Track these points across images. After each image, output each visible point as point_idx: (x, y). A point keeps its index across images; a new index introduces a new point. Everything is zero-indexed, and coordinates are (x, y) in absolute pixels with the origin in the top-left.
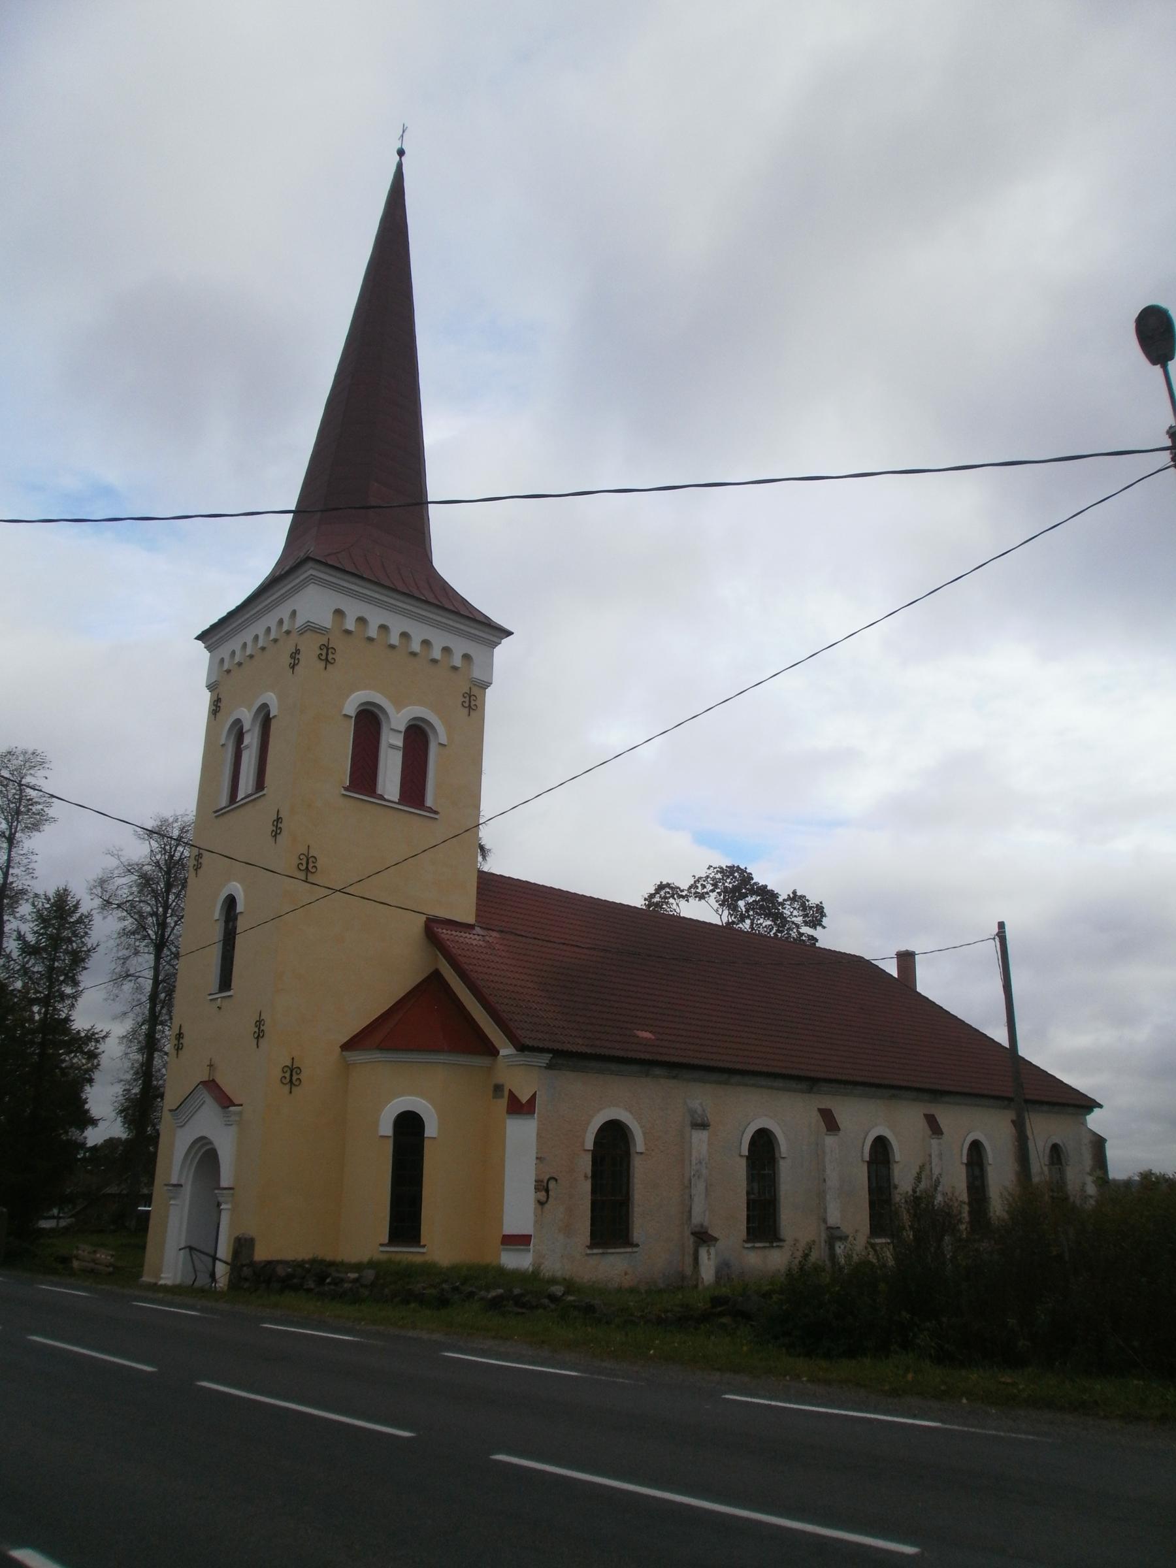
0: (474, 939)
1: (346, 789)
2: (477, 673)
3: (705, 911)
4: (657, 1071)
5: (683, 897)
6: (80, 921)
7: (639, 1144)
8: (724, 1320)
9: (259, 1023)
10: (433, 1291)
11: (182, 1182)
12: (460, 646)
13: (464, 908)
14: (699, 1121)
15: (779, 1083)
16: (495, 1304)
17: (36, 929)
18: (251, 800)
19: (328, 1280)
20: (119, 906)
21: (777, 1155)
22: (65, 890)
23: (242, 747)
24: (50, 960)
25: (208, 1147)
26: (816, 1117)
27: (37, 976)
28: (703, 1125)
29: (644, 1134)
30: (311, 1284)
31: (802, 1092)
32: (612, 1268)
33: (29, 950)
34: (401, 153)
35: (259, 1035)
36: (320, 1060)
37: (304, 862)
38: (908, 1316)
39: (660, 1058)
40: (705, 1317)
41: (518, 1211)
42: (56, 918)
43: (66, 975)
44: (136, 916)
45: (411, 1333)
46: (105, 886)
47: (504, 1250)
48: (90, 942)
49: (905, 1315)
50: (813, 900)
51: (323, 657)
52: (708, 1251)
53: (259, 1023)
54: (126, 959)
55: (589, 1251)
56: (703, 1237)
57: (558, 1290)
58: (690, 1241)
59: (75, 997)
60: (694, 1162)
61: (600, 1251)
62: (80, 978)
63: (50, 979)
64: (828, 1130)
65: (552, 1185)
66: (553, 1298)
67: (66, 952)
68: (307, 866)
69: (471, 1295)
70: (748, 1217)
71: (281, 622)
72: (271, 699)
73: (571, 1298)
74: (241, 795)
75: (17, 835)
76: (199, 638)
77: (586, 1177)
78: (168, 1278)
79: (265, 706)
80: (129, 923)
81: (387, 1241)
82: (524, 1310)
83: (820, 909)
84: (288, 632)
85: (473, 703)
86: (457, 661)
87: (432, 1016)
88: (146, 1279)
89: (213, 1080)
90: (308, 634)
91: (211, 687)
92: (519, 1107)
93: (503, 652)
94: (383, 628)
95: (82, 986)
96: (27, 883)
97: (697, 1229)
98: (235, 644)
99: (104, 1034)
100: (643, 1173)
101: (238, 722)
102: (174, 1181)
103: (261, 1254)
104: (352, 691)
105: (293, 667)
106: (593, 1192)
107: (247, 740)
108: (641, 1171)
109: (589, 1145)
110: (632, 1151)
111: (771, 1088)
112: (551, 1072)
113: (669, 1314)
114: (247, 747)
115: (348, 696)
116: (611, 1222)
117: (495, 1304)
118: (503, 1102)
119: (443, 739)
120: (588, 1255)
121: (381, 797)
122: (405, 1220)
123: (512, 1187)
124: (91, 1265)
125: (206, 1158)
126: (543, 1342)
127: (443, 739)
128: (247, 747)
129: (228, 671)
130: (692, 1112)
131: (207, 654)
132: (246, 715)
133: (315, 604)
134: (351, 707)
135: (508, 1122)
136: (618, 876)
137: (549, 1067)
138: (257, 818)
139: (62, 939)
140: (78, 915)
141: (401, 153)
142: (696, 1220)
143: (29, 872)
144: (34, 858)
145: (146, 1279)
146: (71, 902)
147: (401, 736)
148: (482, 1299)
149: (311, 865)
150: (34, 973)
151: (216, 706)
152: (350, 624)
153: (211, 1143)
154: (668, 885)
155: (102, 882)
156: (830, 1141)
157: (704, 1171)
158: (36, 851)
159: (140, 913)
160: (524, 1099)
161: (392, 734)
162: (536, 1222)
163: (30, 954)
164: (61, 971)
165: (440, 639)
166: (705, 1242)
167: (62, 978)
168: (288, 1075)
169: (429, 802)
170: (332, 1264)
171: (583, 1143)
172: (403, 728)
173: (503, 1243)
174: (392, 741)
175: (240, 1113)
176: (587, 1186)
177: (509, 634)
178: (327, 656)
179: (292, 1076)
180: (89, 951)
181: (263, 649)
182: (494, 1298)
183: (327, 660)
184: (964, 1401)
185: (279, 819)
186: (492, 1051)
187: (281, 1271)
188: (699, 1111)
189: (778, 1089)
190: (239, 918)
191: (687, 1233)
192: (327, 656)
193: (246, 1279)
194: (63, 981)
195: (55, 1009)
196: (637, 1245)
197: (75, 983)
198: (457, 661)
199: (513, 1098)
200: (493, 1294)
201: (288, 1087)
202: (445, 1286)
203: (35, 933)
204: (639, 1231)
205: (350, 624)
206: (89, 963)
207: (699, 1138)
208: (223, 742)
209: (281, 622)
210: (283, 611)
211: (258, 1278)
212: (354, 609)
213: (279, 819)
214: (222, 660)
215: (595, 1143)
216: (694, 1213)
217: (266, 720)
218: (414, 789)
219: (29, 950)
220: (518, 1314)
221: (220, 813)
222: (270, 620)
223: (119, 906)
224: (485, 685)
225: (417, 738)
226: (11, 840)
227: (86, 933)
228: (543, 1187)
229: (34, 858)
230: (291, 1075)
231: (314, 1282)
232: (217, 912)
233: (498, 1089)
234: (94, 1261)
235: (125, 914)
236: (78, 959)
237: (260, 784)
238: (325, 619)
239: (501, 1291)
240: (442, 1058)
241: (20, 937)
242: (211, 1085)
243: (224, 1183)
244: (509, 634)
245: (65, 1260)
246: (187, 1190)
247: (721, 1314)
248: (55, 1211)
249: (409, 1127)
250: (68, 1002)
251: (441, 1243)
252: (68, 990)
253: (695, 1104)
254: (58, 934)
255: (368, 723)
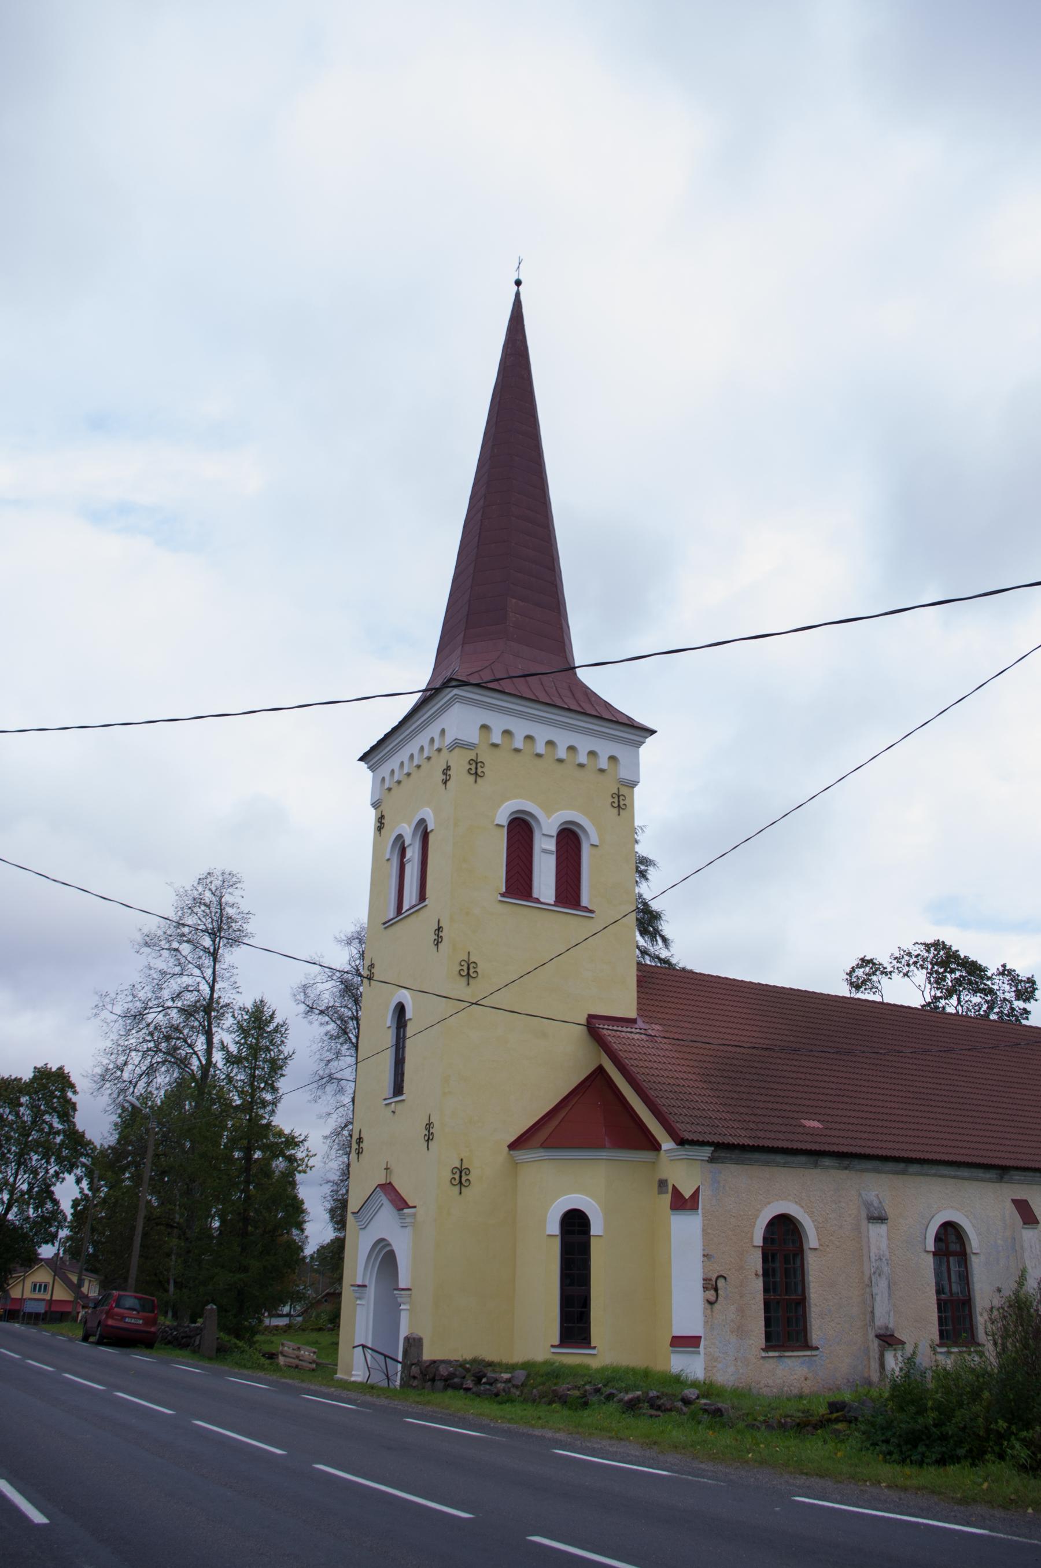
0: (633, 1036)
1: (503, 895)
2: (624, 773)
3: (909, 991)
4: (827, 1162)
5: (886, 974)
6: (276, 1030)
7: (812, 1239)
8: (840, 1426)
9: (429, 1126)
10: (577, 1393)
11: (367, 1283)
12: (605, 749)
13: (624, 1003)
14: (876, 1215)
15: (965, 1172)
16: (632, 1406)
17: (237, 1039)
18: (415, 910)
19: (484, 1380)
20: (322, 1012)
21: (968, 1251)
22: (262, 1001)
23: (406, 861)
24: (251, 1068)
25: (388, 1248)
26: (1010, 1208)
27: (240, 1084)
28: (881, 1219)
29: (817, 1229)
30: (469, 1383)
31: (990, 1181)
32: (789, 1375)
33: (232, 1060)
34: (518, 283)
35: (429, 1138)
36: (488, 1158)
37: (465, 968)
38: (1005, 1425)
39: (827, 1148)
40: (822, 1423)
41: (687, 1313)
42: (254, 1028)
43: (266, 1083)
44: (339, 1022)
45: (537, 1432)
46: (308, 991)
47: (673, 1352)
48: (286, 1050)
49: (1002, 1424)
50: (1023, 974)
51: (473, 771)
52: (895, 1356)
53: (429, 1126)
54: (329, 1061)
55: (764, 1354)
56: (888, 1340)
57: (691, 1393)
58: (875, 1345)
59: (274, 1103)
60: (873, 1260)
61: (776, 1354)
62: (277, 1085)
63: (252, 1085)
64: (1025, 1223)
65: (721, 1283)
66: (686, 1402)
67: (265, 1061)
68: (468, 971)
69: (610, 1397)
70: (940, 1319)
71: (432, 740)
72: (428, 813)
73: (703, 1401)
74: (406, 906)
75: (220, 951)
76: (361, 759)
77: (756, 1275)
78: (358, 1375)
79: (422, 821)
80: (332, 1027)
81: (557, 1342)
82: (659, 1413)
83: (1031, 981)
84: (439, 750)
85: (622, 802)
86: (603, 763)
87: (597, 1114)
88: (339, 1375)
89: (390, 1183)
90: (457, 750)
91: (376, 805)
92: (682, 1203)
93: (648, 751)
94: (529, 738)
95: (281, 1092)
96: (232, 996)
97: (882, 1332)
98: (393, 763)
99: (302, 1138)
100: (819, 1271)
101: (400, 837)
102: (359, 1282)
103: (428, 1354)
104: (503, 802)
105: (445, 782)
106: (766, 1290)
107: (409, 854)
108: (815, 1267)
109: (759, 1240)
110: (805, 1247)
111: (954, 1177)
112: (714, 1165)
113: (788, 1420)
114: (409, 861)
115: (499, 807)
116: (786, 1321)
117: (632, 1406)
118: (667, 1198)
119: (594, 839)
120: (763, 1358)
121: (538, 901)
122: (575, 1323)
123: (677, 1285)
124: (296, 1361)
125: (386, 1259)
126: (655, 1443)
127: (594, 839)
128: (409, 861)
129: (389, 789)
130: (868, 1205)
131: (369, 774)
132: (407, 830)
133: (461, 720)
134: (503, 817)
135: (672, 1217)
136: (810, 960)
137: (712, 1160)
138: (420, 926)
139: (261, 1049)
140: (275, 1025)
141: (518, 283)
142: (879, 1323)
143: (235, 987)
144: (235, 971)
145: (339, 1375)
146: (267, 1013)
147: (554, 841)
148: (620, 1401)
149: (472, 970)
150: (237, 1081)
151: (381, 823)
152: (496, 738)
153: (389, 1245)
154: (871, 961)
155: (305, 988)
156: (1028, 1235)
157: (886, 1269)
158: (236, 965)
159: (341, 1018)
160: (687, 1194)
161: (544, 839)
162: (706, 1322)
163: (233, 1063)
164: (262, 1079)
165: (585, 744)
166: (890, 1345)
167: (262, 1085)
168: (457, 1176)
169: (585, 901)
170: (490, 1364)
171: (752, 1239)
172: (554, 833)
173: (672, 1345)
174: (544, 846)
175: (414, 1215)
176: (759, 1284)
177: (653, 732)
178: (476, 769)
179: (461, 1177)
180: (286, 1058)
181: (419, 767)
182: (631, 1400)
183: (476, 773)
184: (1030, 1511)
185: (439, 929)
186: (655, 1146)
187: (443, 1371)
188: (876, 1203)
189: (963, 1178)
190: (409, 1024)
191: (871, 1335)
192: (476, 769)
193: (414, 1378)
194: (263, 1089)
195: (257, 1114)
196: (817, 1348)
197: (274, 1090)
198: (603, 763)
199: (676, 1193)
200: (630, 1396)
201: (458, 1187)
202: (587, 1387)
203: (237, 1043)
204: (817, 1332)
205: (496, 738)
206: (286, 1071)
207: (877, 1233)
208: (388, 857)
209: (432, 740)
210: (433, 730)
211: (429, 1377)
212: (499, 723)
213: (439, 929)
214: (383, 779)
215: (764, 1238)
216: (877, 1313)
217: (425, 835)
218: (569, 892)
219: (232, 1060)
220: (651, 1416)
221: (388, 924)
222: (422, 739)
223: (322, 1012)
224: (632, 784)
225: (569, 840)
226: (214, 955)
227: (282, 1042)
228: (711, 1285)
229: (235, 971)
230: (461, 1177)
231: (472, 1379)
232: (389, 1019)
233: (662, 1184)
234: (298, 1357)
235: (327, 1019)
236: (276, 1067)
237: (422, 897)
238: (472, 736)
239: (639, 1393)
240: (604, 1154)
241: (224, 1048)
242: (388, 1188)
243: (402, 1285)
244: (653, 732)
245: (272, 1356)
246: (371, 1291)
247: (837, 1420)
248: (286, 1309)
249: (575, 1224)
250: (269, 1108)
251: (609, 1346)
252: (268, 1097)
253: (871, 1196)
254: (257, 1043)
255: (521, 831)
